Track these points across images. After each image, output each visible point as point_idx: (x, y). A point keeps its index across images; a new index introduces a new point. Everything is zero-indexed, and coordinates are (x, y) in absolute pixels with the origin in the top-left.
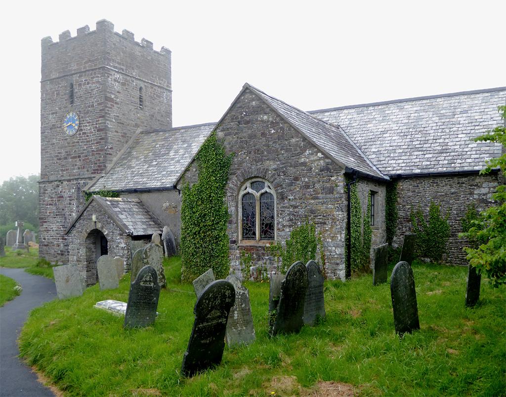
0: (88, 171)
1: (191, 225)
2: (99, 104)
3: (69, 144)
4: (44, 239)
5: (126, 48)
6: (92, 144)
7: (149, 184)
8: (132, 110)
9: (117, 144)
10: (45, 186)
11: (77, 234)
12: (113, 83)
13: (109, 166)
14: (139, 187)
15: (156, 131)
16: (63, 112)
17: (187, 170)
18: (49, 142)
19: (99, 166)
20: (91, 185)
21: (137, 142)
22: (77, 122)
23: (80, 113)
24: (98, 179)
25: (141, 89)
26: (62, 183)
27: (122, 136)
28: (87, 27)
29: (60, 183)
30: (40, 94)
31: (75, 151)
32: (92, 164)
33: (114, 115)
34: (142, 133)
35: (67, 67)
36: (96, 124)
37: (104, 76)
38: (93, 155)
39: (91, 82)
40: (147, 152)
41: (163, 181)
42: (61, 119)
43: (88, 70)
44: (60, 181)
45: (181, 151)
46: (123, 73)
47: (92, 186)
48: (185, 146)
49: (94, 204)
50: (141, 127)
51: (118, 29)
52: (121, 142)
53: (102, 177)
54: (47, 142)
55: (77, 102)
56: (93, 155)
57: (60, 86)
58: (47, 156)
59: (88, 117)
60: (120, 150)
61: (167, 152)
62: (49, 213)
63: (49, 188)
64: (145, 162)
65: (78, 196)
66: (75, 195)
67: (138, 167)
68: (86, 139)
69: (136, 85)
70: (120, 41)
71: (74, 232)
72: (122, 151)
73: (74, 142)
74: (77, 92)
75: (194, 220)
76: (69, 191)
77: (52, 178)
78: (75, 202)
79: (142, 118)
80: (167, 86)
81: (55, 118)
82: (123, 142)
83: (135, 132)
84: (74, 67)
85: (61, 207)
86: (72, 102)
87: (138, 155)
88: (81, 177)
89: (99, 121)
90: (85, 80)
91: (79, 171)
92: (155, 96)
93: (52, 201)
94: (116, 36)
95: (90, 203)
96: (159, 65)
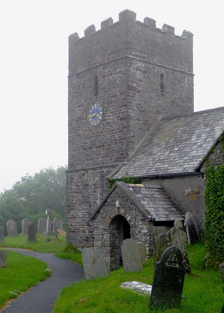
1: (216, 209)
2: (122, 94)
3: (94, 134)
4: (71, 225)
5: (148, 36)
7: (170, 170)
10: (72, 175)
12: (135, 71)
13: (131, 154)
14: (161, 173)
15: (177, 117)
16: (88, 104)
17: (211, 152)
18: (76, 133)
19: (122, 154)
21: (158, 129)
22: (101, 113)
24: (121, 167)
25: (162, 75)
26: (87, 172)
27: (144, 124)
28: (110, 19)
31: (99, 141)
32: (115, 153)
33: (136, 104)
34: (163, 119)
36: (119, 113)
39: (114, 73)
41: (185, 166)
42: (87, 111)
43: (112, 62)
44: (85, 170)
47: (115, 174)
48: (208, 130)
49: (117, 190)
51: (140, 18)
53: (125, 165)
54: (74, 133)
55: (101, 94)
56: (116, 143)
57: (86, 79)
59: (111, 107)
60: (142, 138)
61: (188, 137)
63: (76, 176)
64: (166, 148)
65: (102, 184)
67: (159, 154)
68: (110, 128)
69: (157, 72)
71: (99, 218)
72: (144, 139)
73: (98, 133)
74: (101, 84)
75: (218, 204)
76: (94, 180)
77: (78, 167)
78: (99, 190)
79: (163, 104)
80: (189, 71)
81: (81, 110)
82: (145, 130)
83: (156, 119)
84: (98, 59)
85: (86, 194)
86: (96, 94)
87: (160, 142)
88: (105, 166)
89: (121, 110)
90: (108, 72)
94: (138, 25)
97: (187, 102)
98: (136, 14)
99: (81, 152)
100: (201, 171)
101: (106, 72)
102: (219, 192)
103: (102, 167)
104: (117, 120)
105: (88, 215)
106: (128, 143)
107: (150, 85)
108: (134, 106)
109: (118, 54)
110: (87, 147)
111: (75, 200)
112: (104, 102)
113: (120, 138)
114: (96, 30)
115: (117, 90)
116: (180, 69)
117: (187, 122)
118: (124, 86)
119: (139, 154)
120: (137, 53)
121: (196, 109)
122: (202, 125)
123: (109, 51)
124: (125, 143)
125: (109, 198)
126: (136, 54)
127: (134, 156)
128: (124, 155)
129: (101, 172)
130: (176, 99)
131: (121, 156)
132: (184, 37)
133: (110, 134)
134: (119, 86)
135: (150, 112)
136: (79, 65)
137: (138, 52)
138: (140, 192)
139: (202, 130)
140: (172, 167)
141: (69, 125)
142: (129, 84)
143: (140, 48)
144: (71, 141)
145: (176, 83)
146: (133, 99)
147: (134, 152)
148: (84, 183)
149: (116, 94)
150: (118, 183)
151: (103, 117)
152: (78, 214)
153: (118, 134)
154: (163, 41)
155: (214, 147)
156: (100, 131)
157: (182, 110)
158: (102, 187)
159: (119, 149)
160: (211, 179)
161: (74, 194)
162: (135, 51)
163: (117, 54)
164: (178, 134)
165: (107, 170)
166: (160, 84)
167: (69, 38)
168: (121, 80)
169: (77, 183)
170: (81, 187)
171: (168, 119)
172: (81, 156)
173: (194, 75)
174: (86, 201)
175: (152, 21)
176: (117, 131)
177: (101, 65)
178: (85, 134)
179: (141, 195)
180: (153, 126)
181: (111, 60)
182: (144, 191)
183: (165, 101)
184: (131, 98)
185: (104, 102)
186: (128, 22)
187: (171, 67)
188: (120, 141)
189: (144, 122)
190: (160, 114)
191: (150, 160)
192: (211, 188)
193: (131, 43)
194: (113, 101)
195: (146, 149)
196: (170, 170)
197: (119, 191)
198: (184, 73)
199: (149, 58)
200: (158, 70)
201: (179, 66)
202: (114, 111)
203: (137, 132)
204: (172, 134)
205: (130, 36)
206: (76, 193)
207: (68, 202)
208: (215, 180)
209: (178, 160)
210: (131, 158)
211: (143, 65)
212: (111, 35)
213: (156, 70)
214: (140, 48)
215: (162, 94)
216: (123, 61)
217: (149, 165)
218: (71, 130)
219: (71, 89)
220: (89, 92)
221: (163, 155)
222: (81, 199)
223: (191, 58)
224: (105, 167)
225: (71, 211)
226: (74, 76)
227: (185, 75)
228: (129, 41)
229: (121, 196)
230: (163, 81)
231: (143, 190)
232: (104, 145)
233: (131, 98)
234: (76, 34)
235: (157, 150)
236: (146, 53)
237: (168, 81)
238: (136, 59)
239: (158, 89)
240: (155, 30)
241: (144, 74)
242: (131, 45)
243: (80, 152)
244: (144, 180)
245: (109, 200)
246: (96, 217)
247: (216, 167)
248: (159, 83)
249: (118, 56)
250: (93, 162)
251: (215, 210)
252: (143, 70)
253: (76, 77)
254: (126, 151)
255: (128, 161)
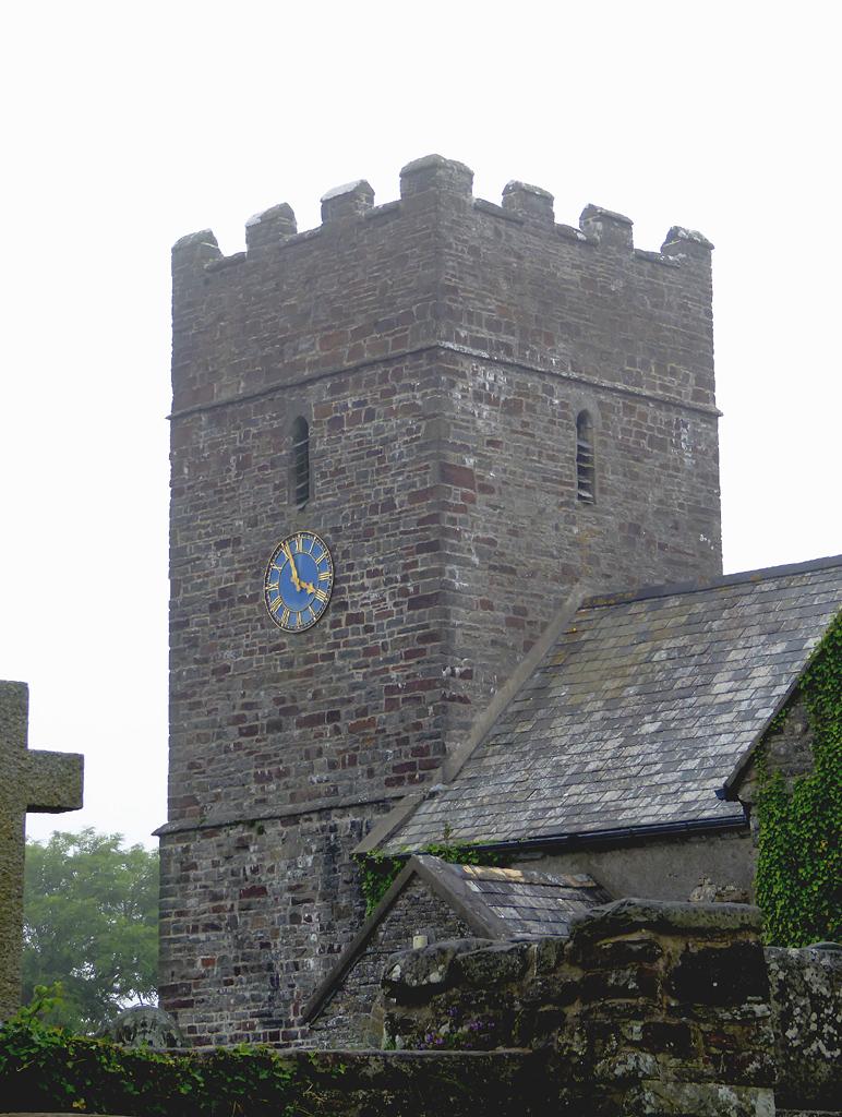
0: (371, 773)
1: (795, 928)
2: (416, 497)
5: (520, 257)
6: (387, 661)
7: (629, 814)
8: (549, 510)
9: (488, 657)
10: (186, 850)
11: (349, 1018)
12: (470, 405)
13: (459, 748)
14: (588, 827)
15: (652, 595)
16: (266, 535)
17: (771, 731)
18: (206, 661)
19: (418, 752)
20: (390, 829)
21: (571, 645)
22: (325, 576)
23: (337, 538)
24: (417, 806)
25: (582, 418)
26: (261, 831)
27: (510, 622)
28: (364, 190)
29: (253, 833)
30: (166, 468)
31: (316, 695)
32: (388, 745)
33: (477, 539)
34: (590, 604)
35: (281, 352)
36: (405, 579)
37: (436, 383)
38: (392, 705)
39: (380, 410)
40: (618, 683)
41: (688, 797)
42: (260, 564)
43: (372, 364)
44: (251, 824)
45: (763, 671)
46: (509, 364)
47: (391, 836)
48: (779, 648)
49: (418, 890)
50: (586, 581)
51: (488, 189)
52: (504, 645)
53: (433, 795)
54: (196, 661)
55: (324, 492)
56: (392, 705)
57: (254, 430)
58: (195, 720)
59: (371, 553)
60: (501, 682)
61: (699, 680)
62: (206, 963)
63: (206, 854)
64: (610, 724)
65: (328, 884)
66: (317, 880)
67: (579, 748)
68: (363, 642)
69: (564, 405)
70: (497, 233)
71: (339, 1010)
72: (511, 684)
73: (314, 659)
74: (323, 454)
75: (803, 909)
76: (293, 865)
77: (216, 814)
78: (315, 912)
79: (590, 540)
80: (698, 396)
81: (230, 562)
82: (514, 648)
83: (559, 603)
84: (310, 351)
85: (253, 933)
86: (303, 495)
87: (579, 699)
88: (344, 801)
89: (414, 564)
90: (355, 404)
91: (332, 775)
92: (644, 442)
93: (215, 910)
94: (479, 217)
95: (404, 889)
96: (657, 312)
97: (691, 528)
98: (470, 175)
99: (232, 746)
100: (740, 797)
101: (345, 407)
102: (804, 867)
103: (331, 808)
104: (396, 605)
105: (265, 1024)
106: (444, 703)
107: (532, 460)
108: (469, 550)
109: (398, 335)
110: (257, 723)
111: (199, 963)
112: (335, 530)
113: (410, 681)
114: (300, 231)
115: (394, 482)
116: (661, 393)
117: (695, 619)
118: (427, 467)
119: (491, 749)
120: (477, 332)
121: (734, 562)
122: (756, 630)
123: (360, 321)
124: (431, 703)
125: (383, 926)
126: (474, 334)
127: (469, 759)
128: (427, 755)
129: (323, 829)
130: (643, 517)
131: (417, 759)
132: (671, 258)
133: (368, 666)
134: (405, 465)
135: (533, 574)
136: (223, 370)
137: (480, 326)
138: (510, 897)
139: (754, 650)
140: (637, 801)
141: (173, 627)
142: (445, 457)
143: (490, 311)
144: (184, 696)
145: (643, 450)
146: (464, 522)
147: (469, 742)
148: (247, 880)
149: (393, 499)
150: (422, 861)
151: (334, 592)
152: (215, 1024)
153: (402, 663)
154: (582, 279)
155: (781, 712)
156: (322, 651)
157: (670, 562)
158: (329, 895)
159: (406, 730)
160: (776, 823)
161: (194, 936)
162: (471, 322)
163: (396, 332)
164: (658, 667)
165: (353, 823)
166: (575, 457)
167: (175, 250)
168: (413, 440)
169: (209, 883)
170: (228, 903)
171: (613, 602)
172: (231, 760)
173: (721, 415)
174: (254, 964)
175: (540, 196)
176: (397, 653)
177: (326, 376)
178: (251, 665)
179: (513, 911)
180: (549, 631)
181: (367, 356)
182: (524, 897)
183: (599, 524)
184: (454, 515)
185: (335, 530)
186: (442, 209)
187: (620, 386)
188: (408, 695)
189: (511, 615)
190: (577, 580)
191: (543, 773)
192: (778, 854)
193: (454, 290)
194: (380, 528)
195: (523, 730)
196: (629, 814)
197: (424, 895)
198: (675, 405)
199: (527, 348)
200: (568, 396)
201: (654, 377)
202: (380, 567)
203: (482, 656)
204: (630, 666)
205: (451, 263)
206: (204, 930)
207: (168, 973)
208: (791, 826)
209: (657, 773)
210: (460, 764)
211: (503, 380)
212: (369, 256)
213: (558, 398)
214: (490, 311)
215: (585, 498)
216: (421, 366)
217: (538, 795)
218: (181, 646)
219: (186, 470)
220: (271, 486)
221: (596, 754)
222: (232, 956)
223: (706, 341)
224: (343, 808)
225: (180, 1011)
226: (197, 415)
227: (681, 414)
228: (447, 283)
229: (434, 914)
230: (587, 441)
231: (520, 892)
232: (338, 711)
233: (454, 515)
234: (208, 237)
235: (571, 732)
236: (515, 328)
237: (611, 442)
238: (476, 357)
239: (567, 476)
240: (553, 232)
241: (508, 418)
242: (455, 301)
243: (225, 743)
244: (522, 856)
245: (381, 934)
246: (328, 1005)
247: (792, 781)
248: (571, 453)
249: (398, 343)
250: (288, 788)
251: (793, 934)
252: (502, 399)
253: (210, 422)
254: (438, 736)
255: (444, 779)
